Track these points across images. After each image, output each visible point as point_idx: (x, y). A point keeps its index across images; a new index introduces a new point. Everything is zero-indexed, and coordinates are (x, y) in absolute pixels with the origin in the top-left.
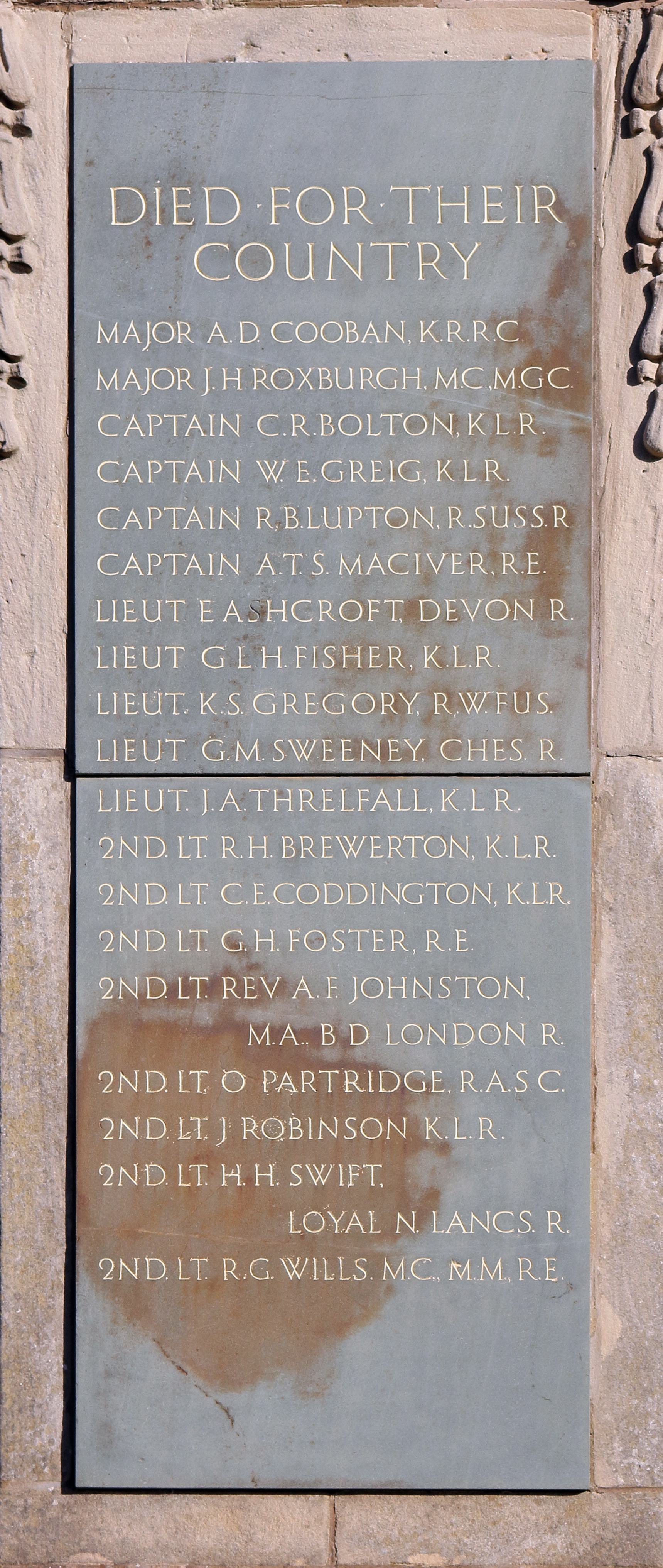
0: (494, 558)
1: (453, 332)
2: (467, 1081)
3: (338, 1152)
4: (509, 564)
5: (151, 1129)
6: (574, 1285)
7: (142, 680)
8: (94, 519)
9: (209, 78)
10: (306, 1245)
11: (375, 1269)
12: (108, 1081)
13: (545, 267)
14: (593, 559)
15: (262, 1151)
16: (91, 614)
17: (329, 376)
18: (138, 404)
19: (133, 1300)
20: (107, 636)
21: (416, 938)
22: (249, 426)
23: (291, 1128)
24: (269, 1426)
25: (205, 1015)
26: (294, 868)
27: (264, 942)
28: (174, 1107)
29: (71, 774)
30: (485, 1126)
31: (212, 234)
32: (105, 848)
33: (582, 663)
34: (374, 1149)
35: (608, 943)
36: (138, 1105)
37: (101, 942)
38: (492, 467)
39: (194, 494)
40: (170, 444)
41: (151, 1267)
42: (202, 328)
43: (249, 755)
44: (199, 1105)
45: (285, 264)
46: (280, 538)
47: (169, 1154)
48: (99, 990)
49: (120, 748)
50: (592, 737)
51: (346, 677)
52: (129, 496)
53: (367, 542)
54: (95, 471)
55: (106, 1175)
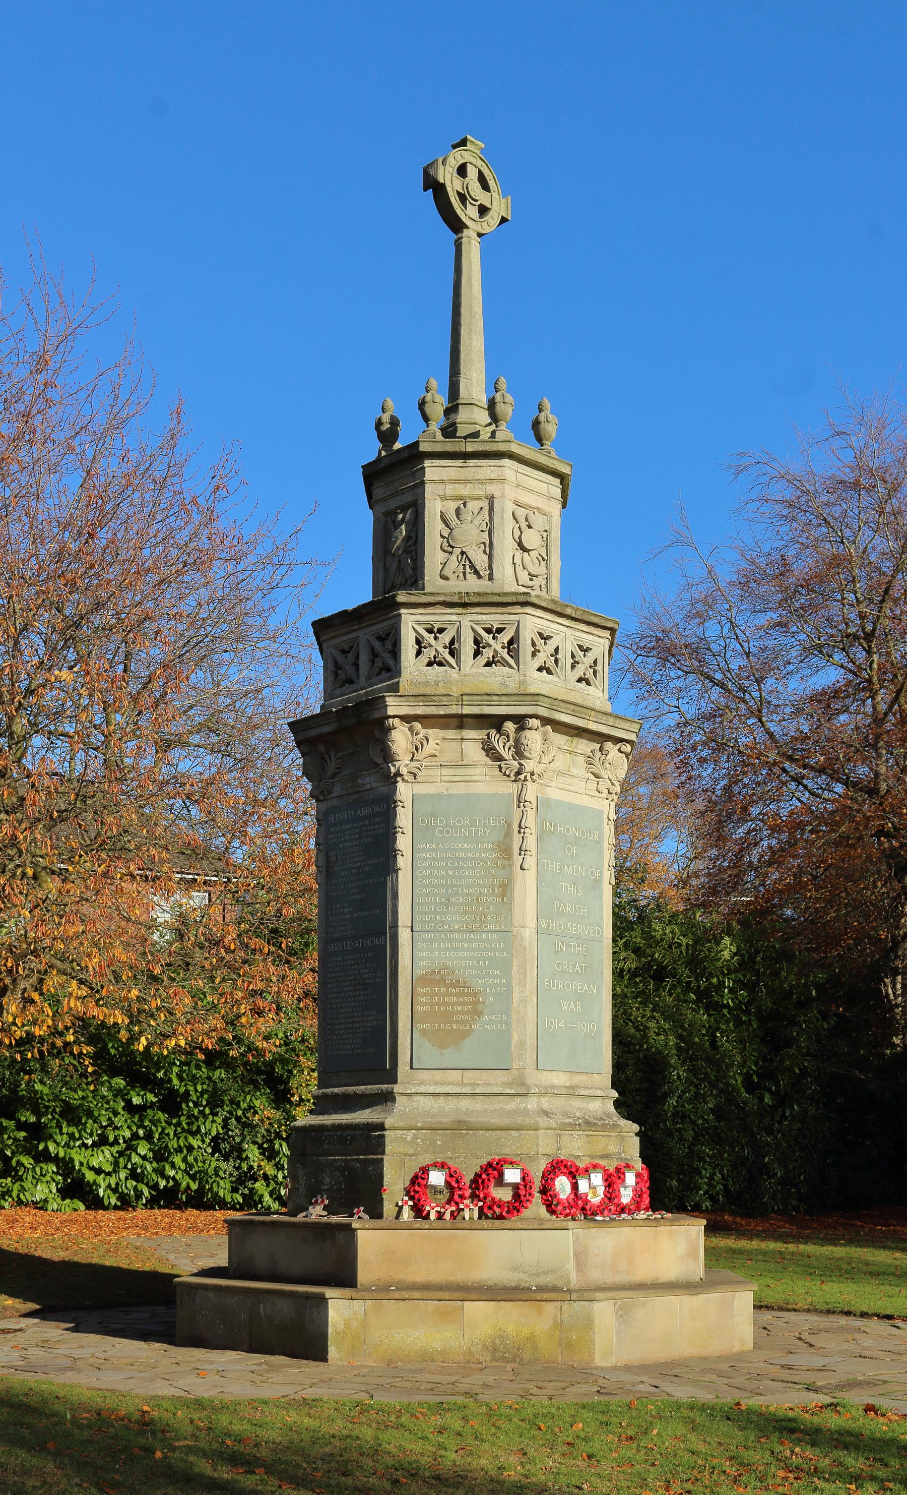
0: (493, 890)
1: (486, 846)
2: (488, 990)
3: (463, 1004)
4: (496, 891)
5: (427, 999)
6: (508, 1030)
7: (426, 913)
8: (417, 882)
9: (439, 796)
10: (457, 1022)
11: (470, 1027)
12: (420, 990)
13: (503, 833)
14: (512, 889)
15: (449, 1004)
16: (416, 900)
17: (462, 855)
18: (425, 860)
19: (424, 1032)
20: (420, 905)
21: (478, 963)
22: (446, 864)
23: (455, 999)
24: (450, 1057)
25: (438, 977)
26: (455, 949)
27: (449, 963)
28: (432, 995)
29: (412, 931)
30: (492, 999)
31: (440, 827)
32: (419, 945)
33: (510, 910)
34: (470, 1004)
35: (515, 963)
36: (425, 995)
37: (419, 963)
38: (493, 872)
39: (436, 877)
40: (431, 867)
41: (427, 1026)
42: (438, 845)
43: (446, 927)
44: (436, 995)
45: (563, 557)
46: (452, 886)
47: (431, 1004)
48: (418, 972)
49: (455, 722)
50: (512, 924)
51: (465, 912)
52: (424, 877)
53: (469, 886)
54: (417, 873)
55: (419, 1008)
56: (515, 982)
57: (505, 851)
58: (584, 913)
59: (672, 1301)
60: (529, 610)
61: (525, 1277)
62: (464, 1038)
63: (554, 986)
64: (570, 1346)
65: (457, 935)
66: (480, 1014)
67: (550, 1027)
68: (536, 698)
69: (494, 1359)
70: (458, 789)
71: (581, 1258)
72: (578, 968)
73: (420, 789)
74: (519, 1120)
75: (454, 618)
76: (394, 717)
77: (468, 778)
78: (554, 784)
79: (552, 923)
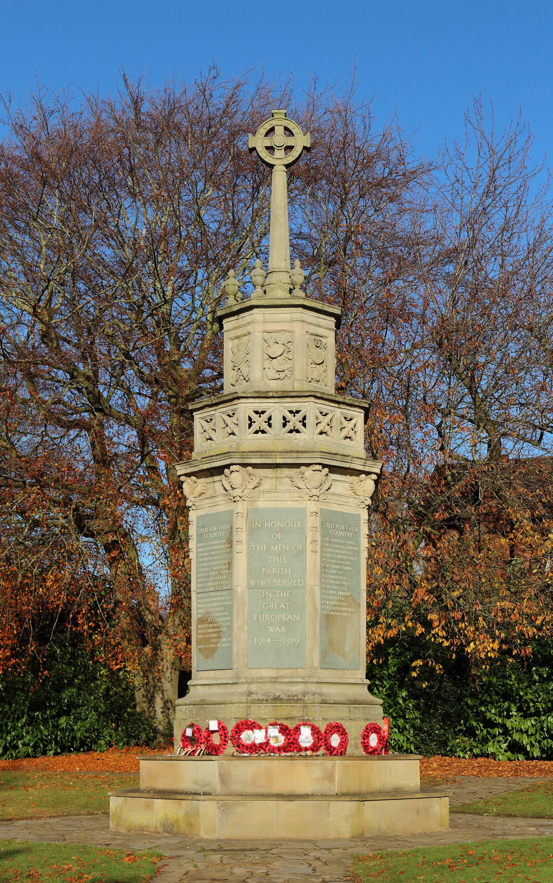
10: (212, 643)
27: (209, 610)
56: (235, 618)
57: (230, 542)
58: (288, 572)
59: (271, 804)
60: (241, 401)
61: (198, 787)
62: (214, 652)
63: (262, 618)
64: (190, 825)
65: (212, 594)
66: (221, 638)
67: (258, 643)
68: (230, 454)
69: (164, 831)
70: (214, 510)
71: (224, 778)
72: (282, 605)
73: (200, 513)
74: (228, 699)
75: (213, 412)
76: (181, 475)
77: (216, 504)
78: (261, 499)
79: (260, 581)
